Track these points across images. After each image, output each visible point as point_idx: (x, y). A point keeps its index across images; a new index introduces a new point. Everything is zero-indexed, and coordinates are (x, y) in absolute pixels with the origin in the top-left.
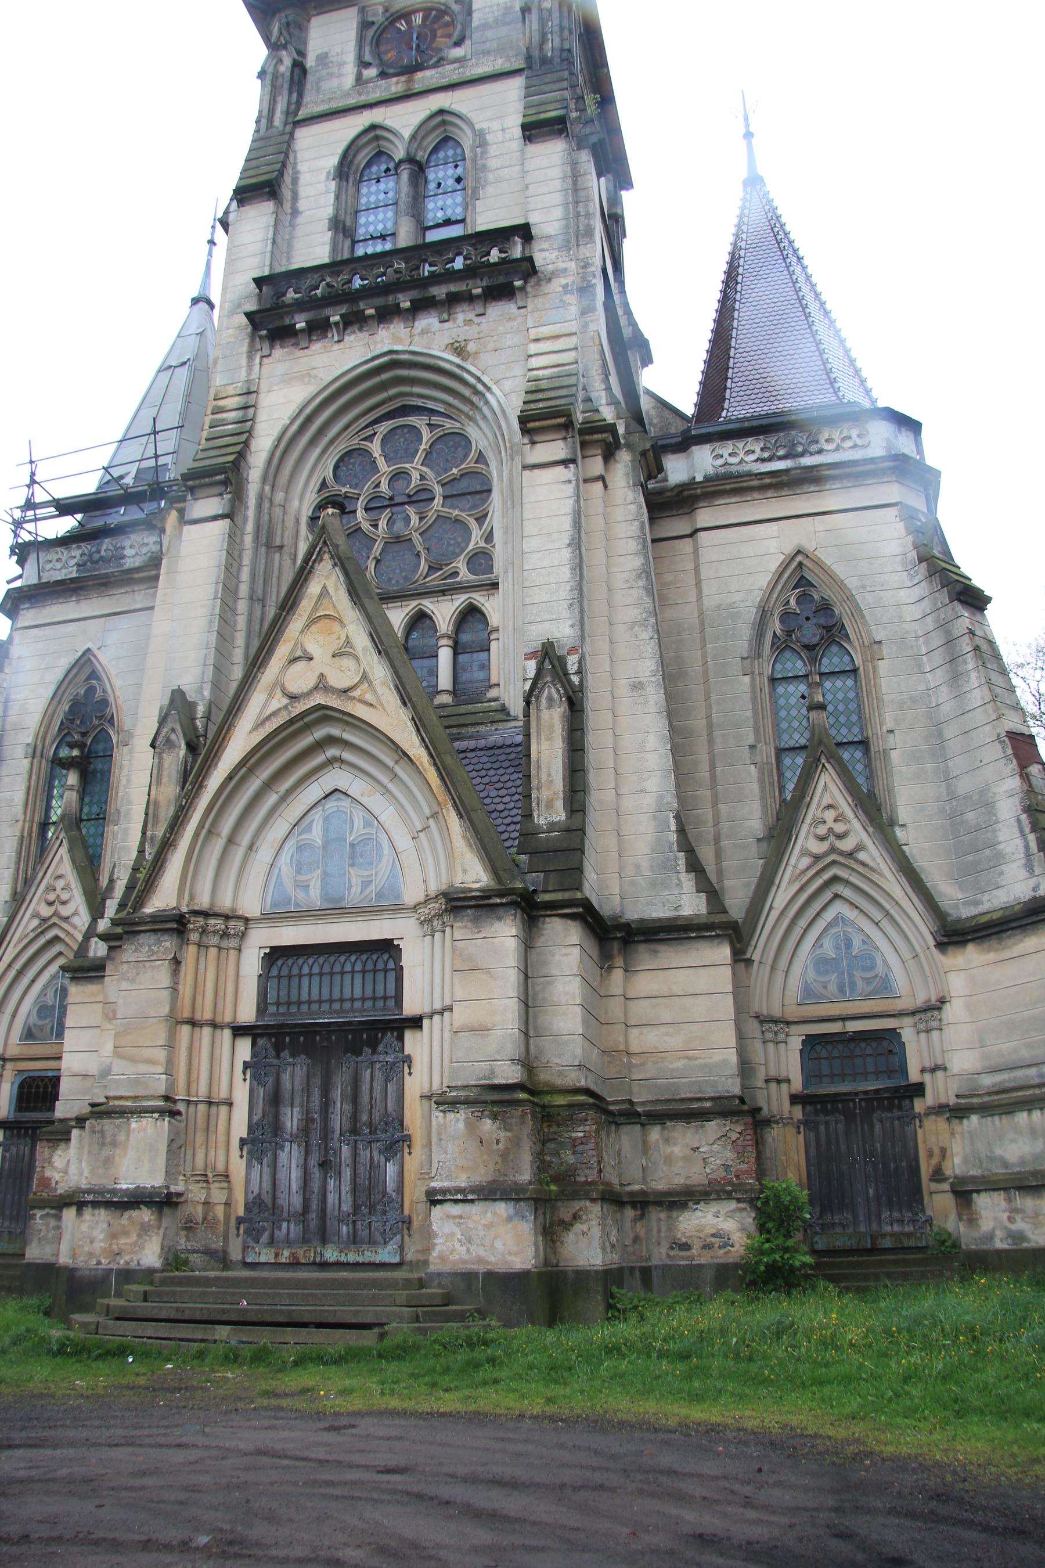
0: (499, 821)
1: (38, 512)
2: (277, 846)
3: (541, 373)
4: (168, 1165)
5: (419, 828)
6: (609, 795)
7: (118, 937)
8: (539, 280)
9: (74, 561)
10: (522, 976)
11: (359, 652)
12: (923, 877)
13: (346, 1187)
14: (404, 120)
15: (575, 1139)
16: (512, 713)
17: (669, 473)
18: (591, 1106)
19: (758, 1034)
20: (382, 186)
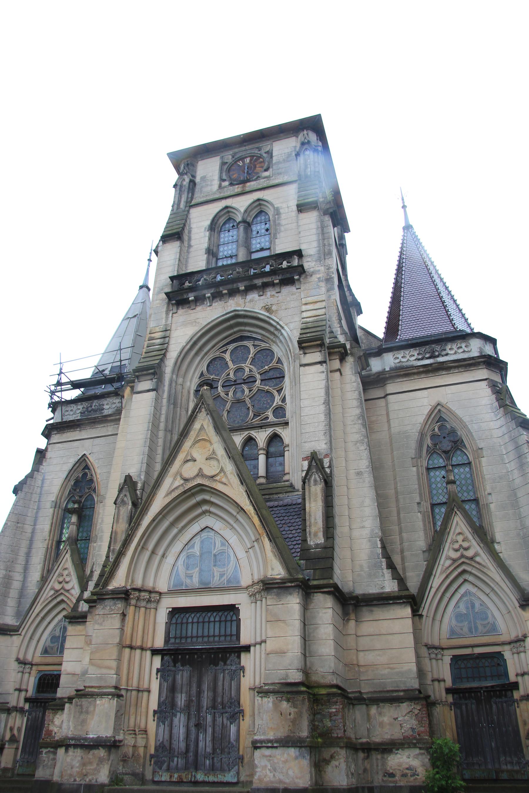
0: (290, 543)
1: (63, 387)
2: (177, 555)
3: (308, 320)
4: (115, 724)
5: (249, 546)
6: (346, 529)
7: (94, 601)
8: (307, 276)
9: (79, 411)
10: (302, 624)
11: (219, 457)
12: (511, 570)
13: (209, 738)
14: (241, 204)
15: (331, 713)
16: (296, 488)
17: (372, 367)
18: (339, 695)
19: (427, 655)
20: (231, 233)
